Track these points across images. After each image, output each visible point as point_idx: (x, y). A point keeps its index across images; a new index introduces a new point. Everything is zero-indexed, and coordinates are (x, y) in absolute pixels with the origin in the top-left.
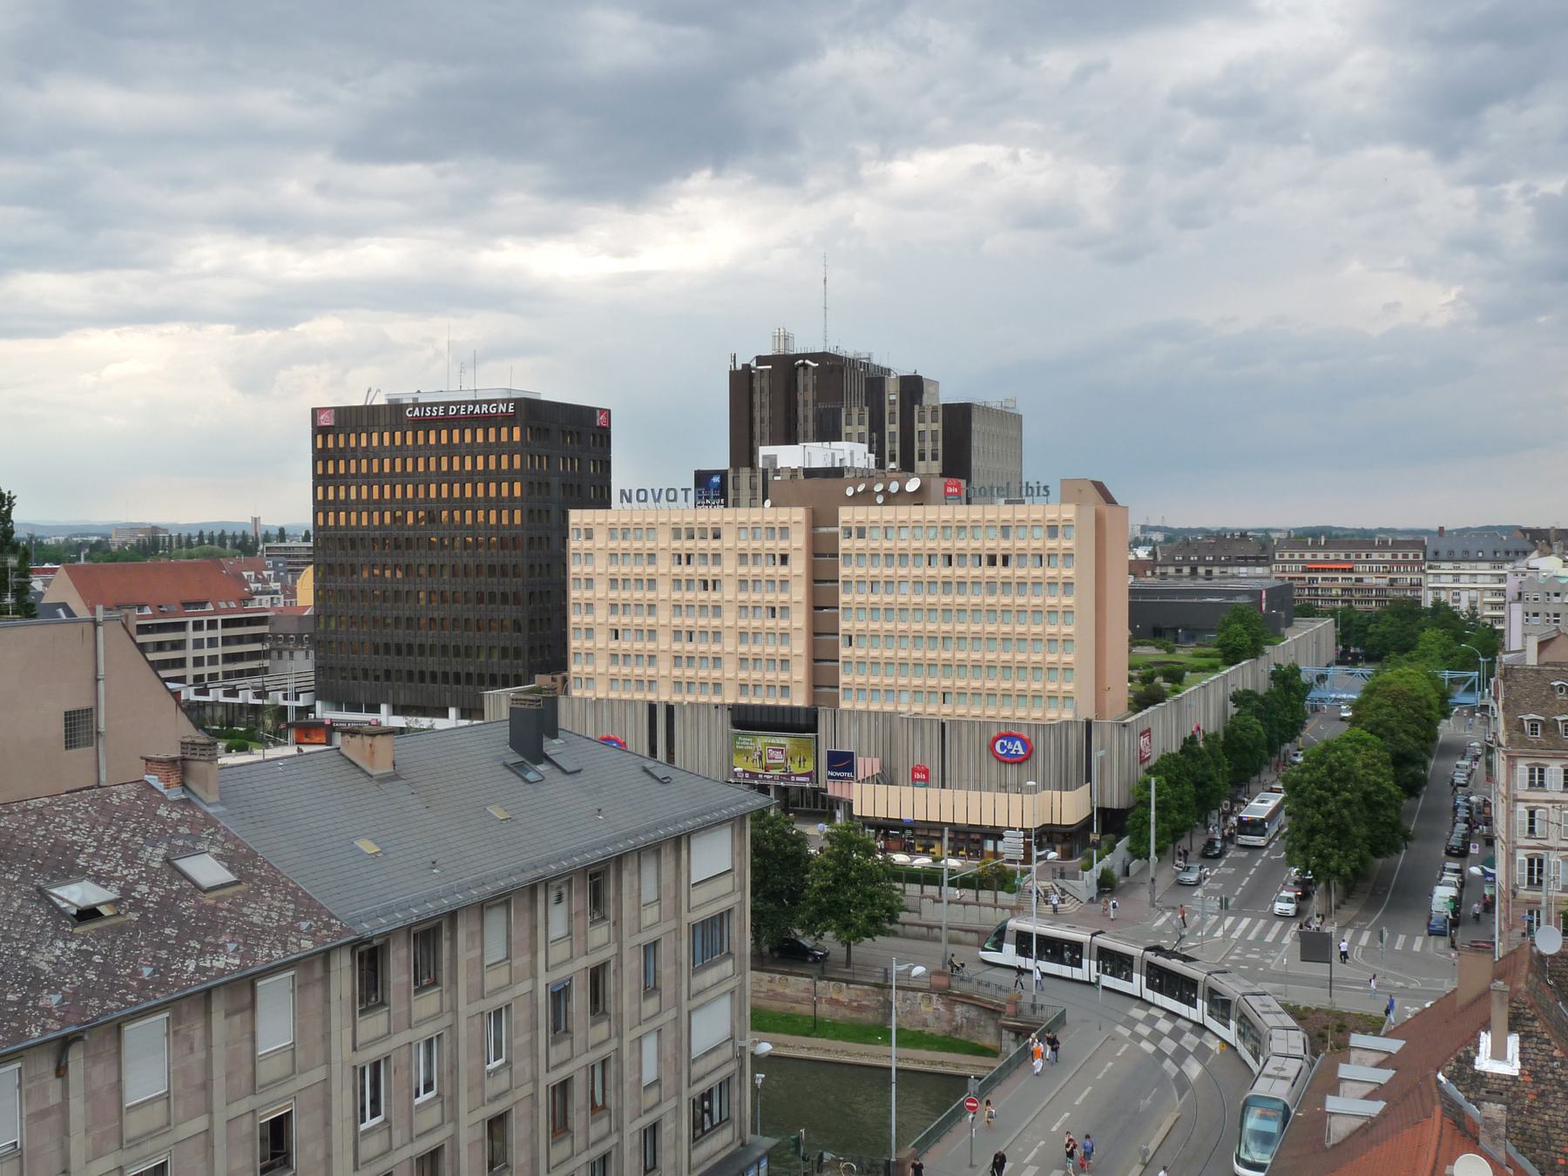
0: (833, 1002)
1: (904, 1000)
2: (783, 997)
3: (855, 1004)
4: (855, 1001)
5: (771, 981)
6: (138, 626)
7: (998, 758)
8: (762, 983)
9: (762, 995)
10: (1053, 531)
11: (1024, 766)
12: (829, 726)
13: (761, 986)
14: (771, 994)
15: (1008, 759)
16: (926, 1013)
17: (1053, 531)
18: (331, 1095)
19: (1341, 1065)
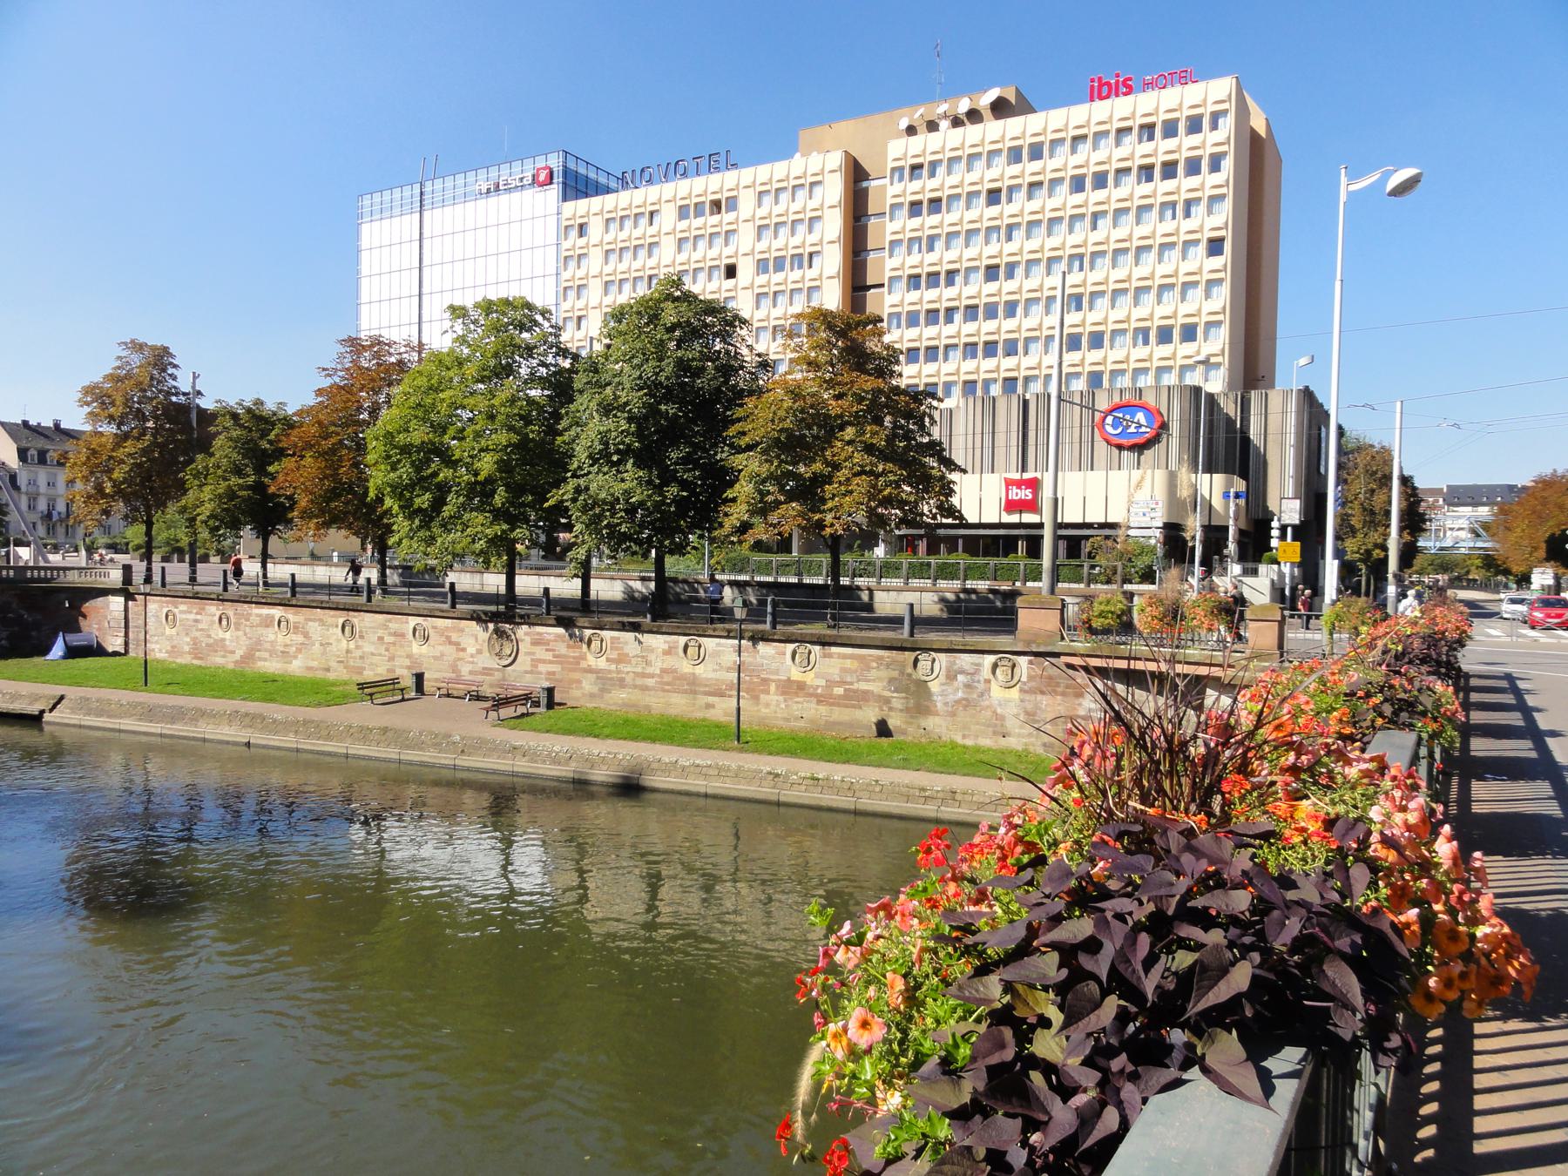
0: (792, 688)
1: (951, 676)
2: (692, 686)
3: (839, 691)
4: (842, 683)
5: (667, 652)
6: (1069, 557)
7: (1108, 442)
8: (652, 657)
9: (650, 682)
10: (994, 196)
11: (1148, 454)
12: (986, 437)
13: (648, 663)
14: (667, 678)
15: (1124, 441)
16: (1004, 703)
17: (994, 196)
18: (847, 762)
19: (868, 311)
